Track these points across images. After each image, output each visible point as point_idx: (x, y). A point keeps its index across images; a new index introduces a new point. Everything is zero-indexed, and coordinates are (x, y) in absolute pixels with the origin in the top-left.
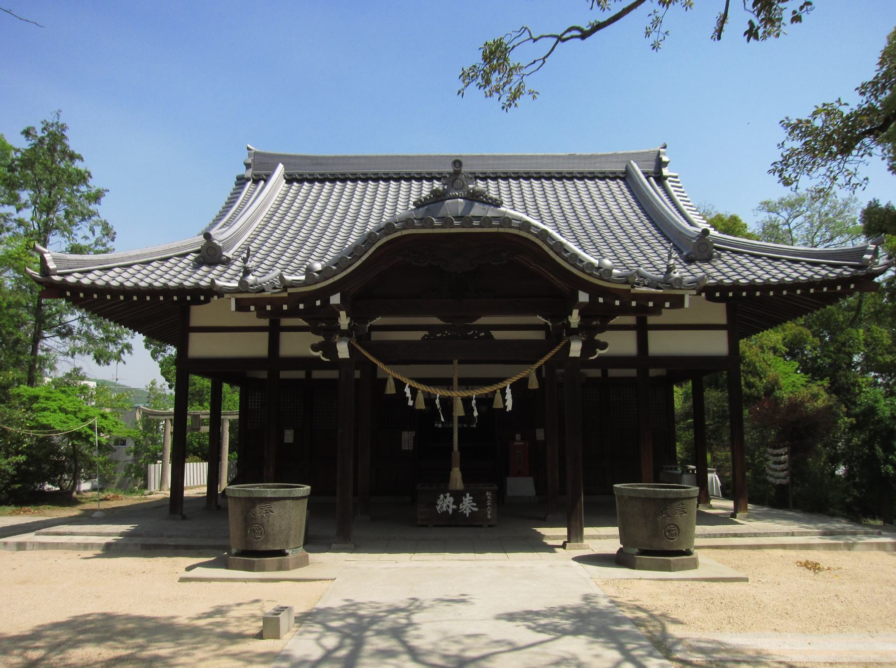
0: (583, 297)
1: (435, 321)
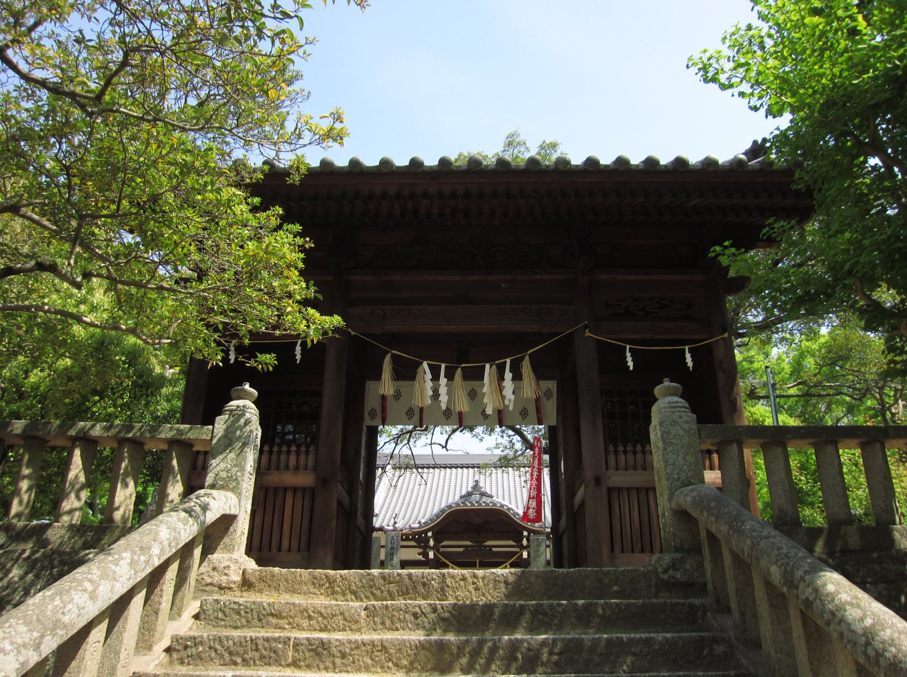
0: (525, 533)
1: (468, 543)
